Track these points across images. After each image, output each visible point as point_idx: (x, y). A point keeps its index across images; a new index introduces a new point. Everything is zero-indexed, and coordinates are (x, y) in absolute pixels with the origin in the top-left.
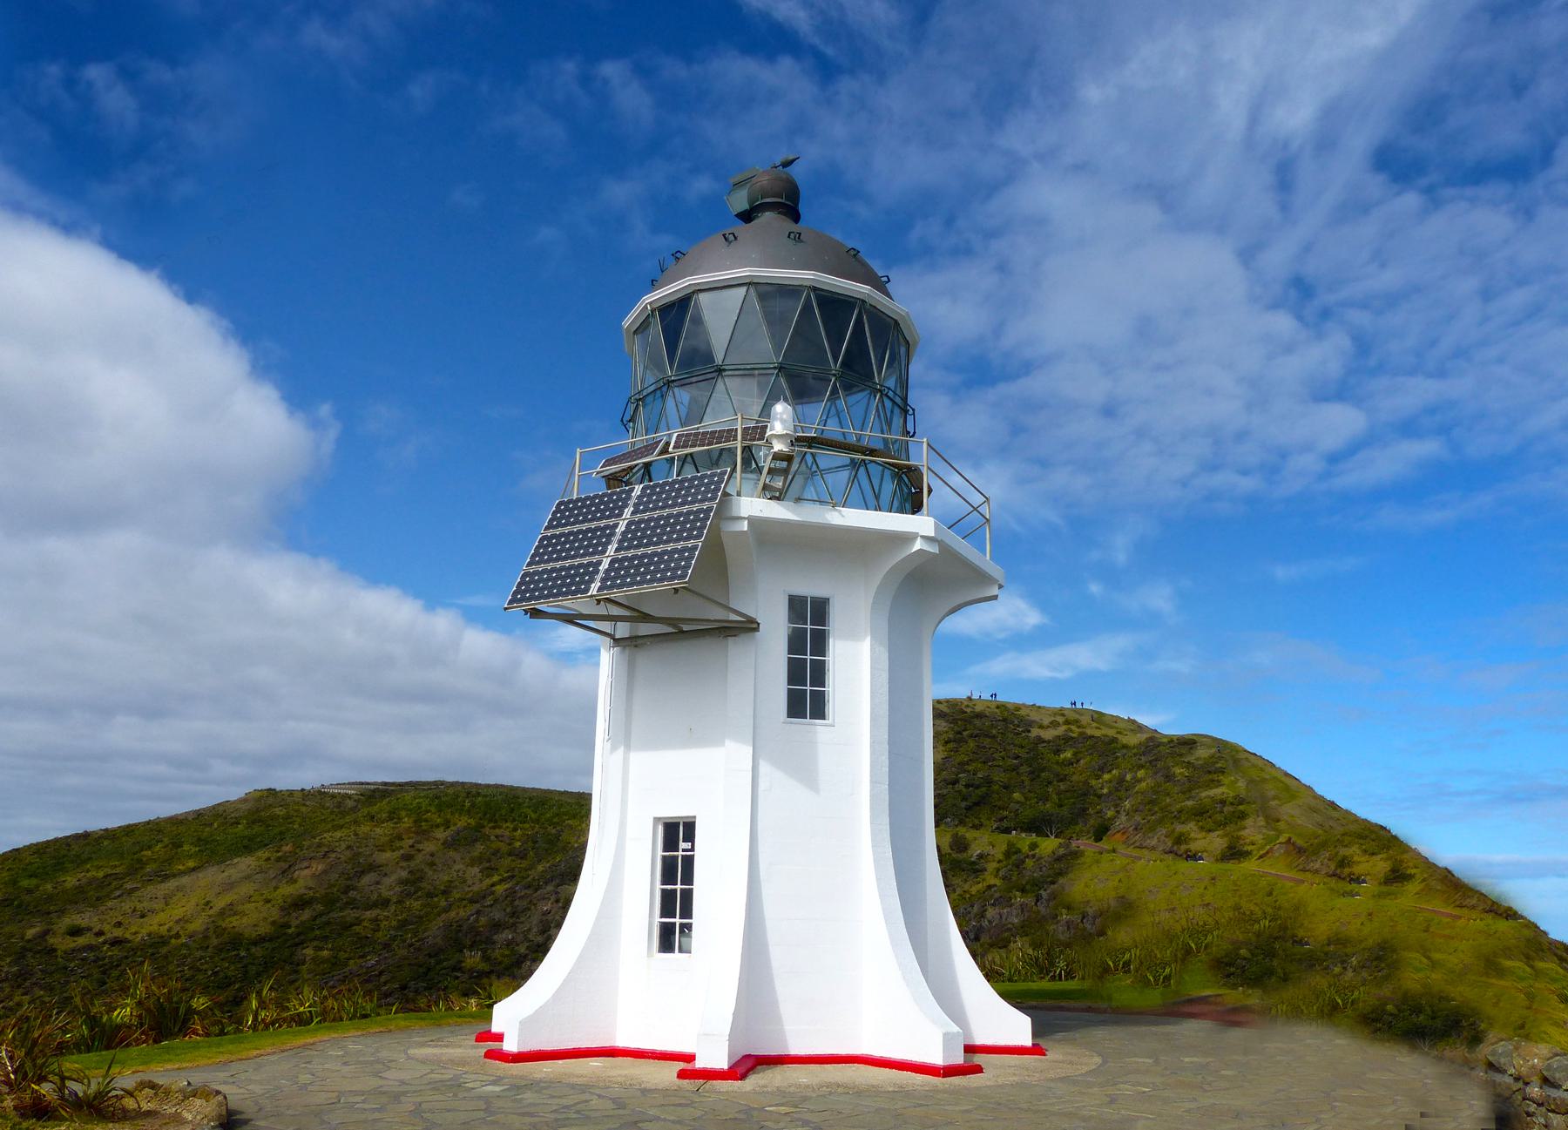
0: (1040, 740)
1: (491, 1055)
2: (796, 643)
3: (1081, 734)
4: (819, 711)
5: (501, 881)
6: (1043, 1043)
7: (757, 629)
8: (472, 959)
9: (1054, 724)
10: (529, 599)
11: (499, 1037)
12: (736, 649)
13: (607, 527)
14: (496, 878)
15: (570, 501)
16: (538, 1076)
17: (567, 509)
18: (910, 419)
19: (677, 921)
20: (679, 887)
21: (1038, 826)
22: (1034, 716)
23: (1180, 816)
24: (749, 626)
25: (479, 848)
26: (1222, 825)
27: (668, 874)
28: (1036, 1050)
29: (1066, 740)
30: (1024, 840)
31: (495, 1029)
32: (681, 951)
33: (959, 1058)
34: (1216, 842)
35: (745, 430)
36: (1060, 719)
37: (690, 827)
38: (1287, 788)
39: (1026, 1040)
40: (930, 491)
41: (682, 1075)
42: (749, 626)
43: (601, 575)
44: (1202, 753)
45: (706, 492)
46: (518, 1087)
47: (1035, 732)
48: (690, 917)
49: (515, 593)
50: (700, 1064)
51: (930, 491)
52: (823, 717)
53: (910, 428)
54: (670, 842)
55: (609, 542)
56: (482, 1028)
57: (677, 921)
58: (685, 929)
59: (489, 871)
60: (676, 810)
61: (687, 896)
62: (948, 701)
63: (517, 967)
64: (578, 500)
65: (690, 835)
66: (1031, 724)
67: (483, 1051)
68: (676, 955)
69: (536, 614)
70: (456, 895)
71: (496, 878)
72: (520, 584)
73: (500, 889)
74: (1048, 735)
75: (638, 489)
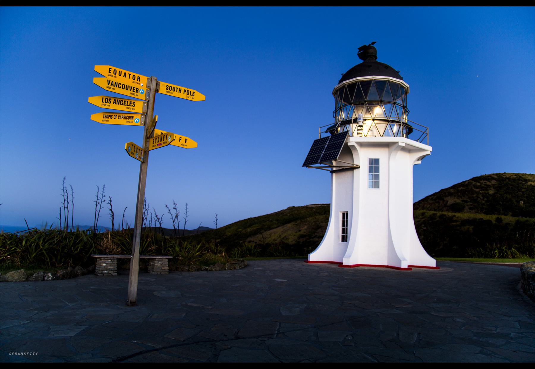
2: (371, 170)
24: (358, 167)
33: (407, 267)
37: (347, 214)
42: (358, 167)
47: (530, 183)
54: (343, 218)
65: (378, 164)
66: (529, 180)
69: (309, 167)
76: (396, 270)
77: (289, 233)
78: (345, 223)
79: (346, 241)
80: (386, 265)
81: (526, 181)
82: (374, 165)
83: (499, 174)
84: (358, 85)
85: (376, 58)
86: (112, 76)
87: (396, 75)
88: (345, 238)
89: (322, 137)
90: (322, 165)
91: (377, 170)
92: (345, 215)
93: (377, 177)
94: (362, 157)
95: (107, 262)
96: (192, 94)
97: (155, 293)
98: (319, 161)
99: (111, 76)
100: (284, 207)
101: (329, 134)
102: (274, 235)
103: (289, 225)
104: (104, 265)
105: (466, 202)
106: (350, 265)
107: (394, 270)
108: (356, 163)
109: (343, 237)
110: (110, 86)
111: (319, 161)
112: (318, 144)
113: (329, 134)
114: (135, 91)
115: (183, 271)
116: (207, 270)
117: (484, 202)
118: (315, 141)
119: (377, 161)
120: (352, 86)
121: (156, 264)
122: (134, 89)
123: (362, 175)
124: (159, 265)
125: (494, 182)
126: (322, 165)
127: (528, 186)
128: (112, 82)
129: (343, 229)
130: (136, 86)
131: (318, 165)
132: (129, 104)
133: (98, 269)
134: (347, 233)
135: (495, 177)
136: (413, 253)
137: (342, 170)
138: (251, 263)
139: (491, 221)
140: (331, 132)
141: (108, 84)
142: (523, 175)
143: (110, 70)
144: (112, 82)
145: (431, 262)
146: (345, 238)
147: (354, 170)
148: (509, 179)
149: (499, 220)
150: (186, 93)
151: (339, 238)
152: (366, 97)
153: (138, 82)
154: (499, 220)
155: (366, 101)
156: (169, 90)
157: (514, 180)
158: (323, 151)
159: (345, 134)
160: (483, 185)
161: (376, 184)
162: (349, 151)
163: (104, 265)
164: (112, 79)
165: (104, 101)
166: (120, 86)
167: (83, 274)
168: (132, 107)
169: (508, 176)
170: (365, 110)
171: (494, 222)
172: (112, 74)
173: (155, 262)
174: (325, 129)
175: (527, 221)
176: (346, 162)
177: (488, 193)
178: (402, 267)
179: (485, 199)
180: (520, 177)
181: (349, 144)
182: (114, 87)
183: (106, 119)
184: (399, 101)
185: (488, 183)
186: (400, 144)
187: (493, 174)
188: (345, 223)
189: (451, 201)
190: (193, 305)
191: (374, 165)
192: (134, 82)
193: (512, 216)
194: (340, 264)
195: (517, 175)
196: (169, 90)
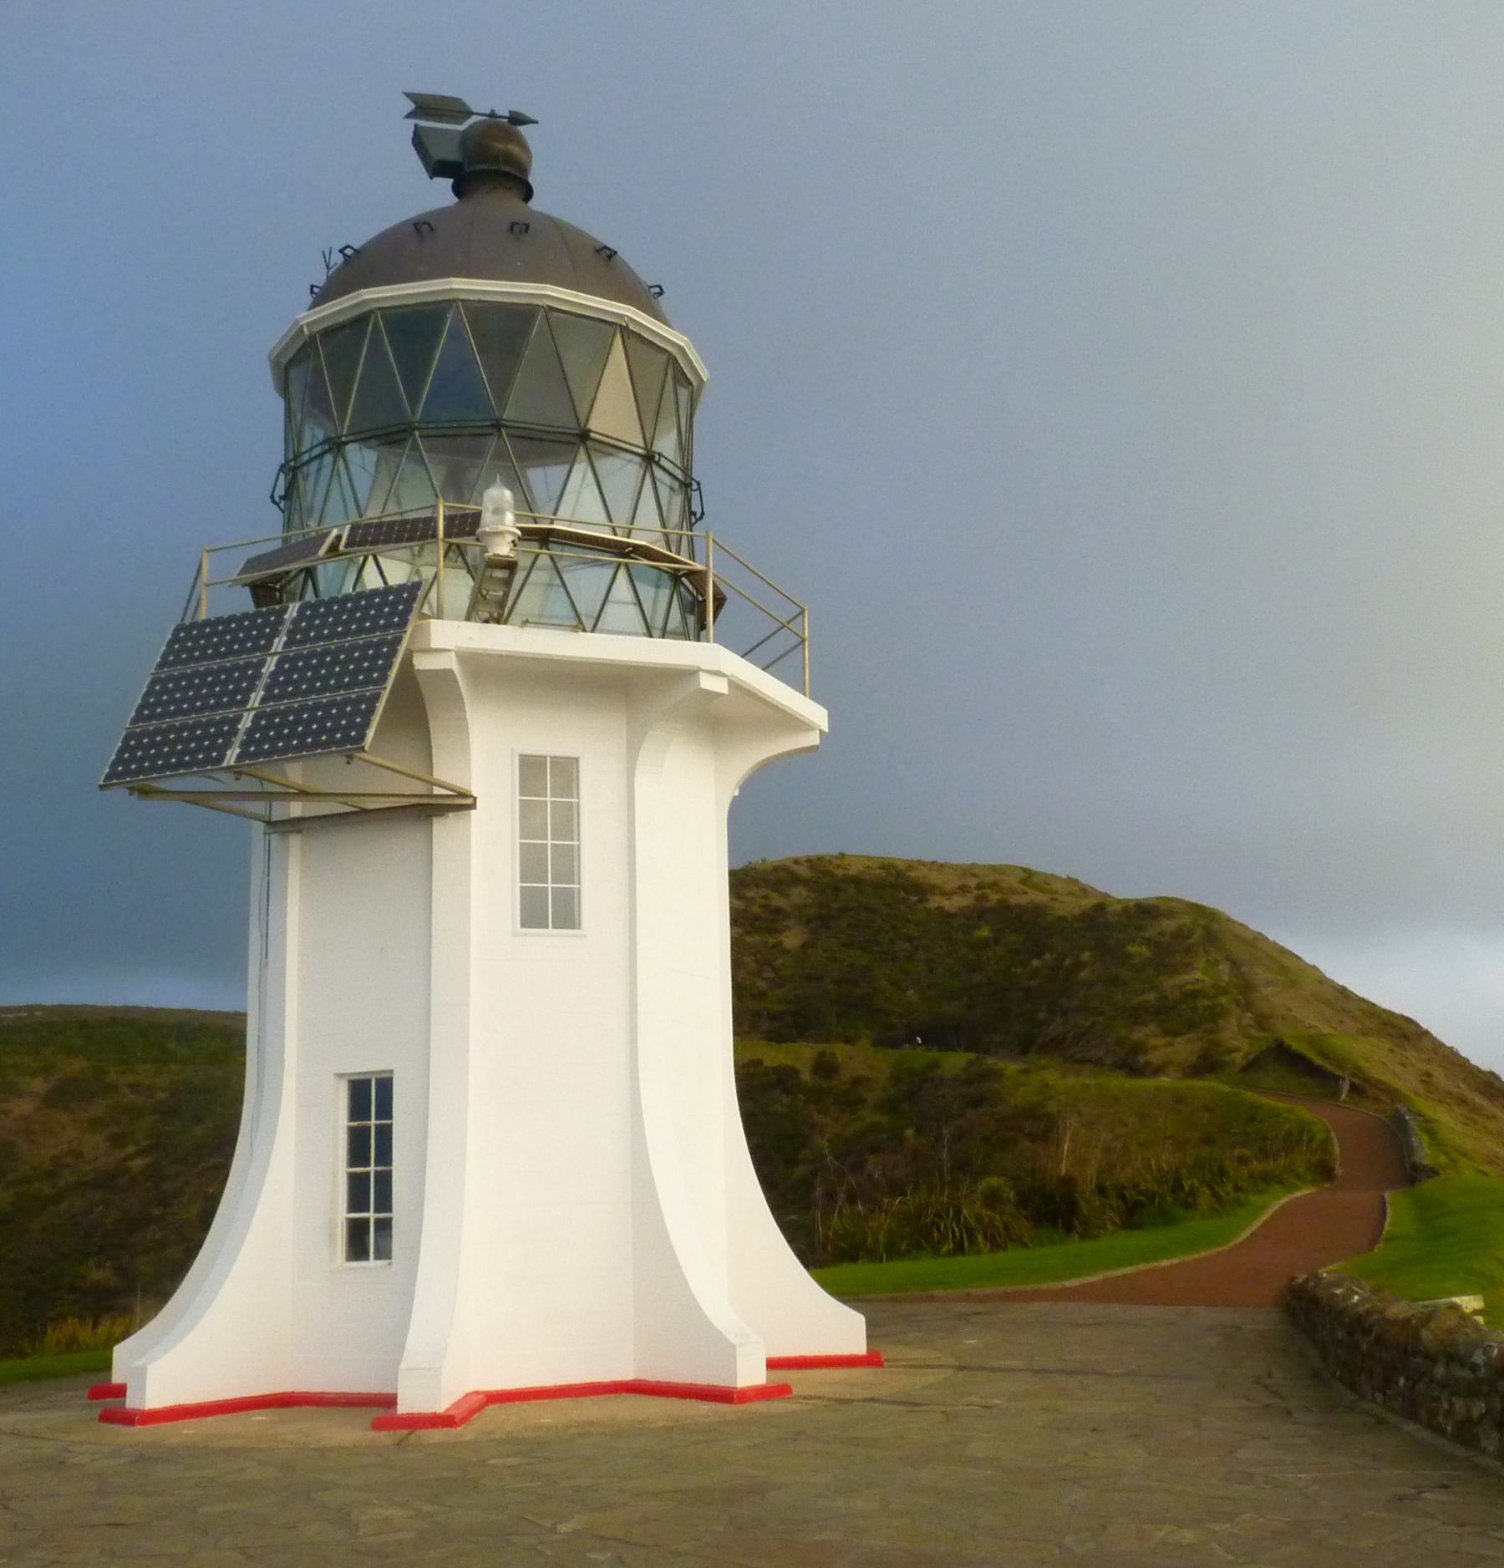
0: (945, 916)
1: (108, 1417)
3: (1000, 902)
4: (567, 915)
5: (139, 1153)
6: (887, 1352)
8: (99, 1274)
9: (963, 889)
10: (136, 773)
11: (121, 1391)
12: (443, 829)
13: (248, 666)
14: (131, 1149)
15: (193, 625)
16: (174, 1441)
17: (189, 637)
18: (695, 496)
19: (372, 1215)
20: (372, 1169)
21: (940, 1036)
22: (934, 878)
23: (1136, 1016)
24: (460, 803)
25: (99, 1107)
26: (1191, 1026)
27: (358, 1149)
28: (870, 1360)
29: (979, 914)
30: (918, 1056)
31: (117, 1378)
32: (378, 1257)
34: (1184, 1048)
35: (449, 520)
36: (973, 882)
37: (385, 1085)
38: (1284, 970)
39: (860, 1348)
40: (720, 601)
41: (378, 1425)
42: (460, 803)
43: (240, 737)
44: (1169, 925)
45: (392, 614)
46: (143, 1458)
47: (935, 902)
48: (389, 1209)
49: (115, 764)
50: (403, 1408)
51: (720, 601)
52: (567, 915)
53: (696, 507)
54: (358, 1108)
55: (252, 688)
56: (96, 1380)
57: (372, 1215)
58: (384, 1226)
59: (117, 1140)
60: (367, 1064)
61: (385, 1180)
62: (809, 861)
64: (207, 623)
65: (385, 1110)
66: (933, 889)
67: (97, 1412)
68: (372, 1262)
69: (145, 792)
70: (68, 1177)
71: (131, 1149)
72: (121, 752)
73: (138, 1164)
74: (954, 904)
75: (293, 610)
76: (705, 1407)
79: (384, 1253)
80: (627, 1374)
81: (922, 890)
83: (820, 858)
85: (528, 193)
87: (647, 298)
92: (370, 1099)
94: (484, 753)
108: (447, 772)
117: (761, 984)
119: (566, 770)
120: (416, 327)
123: (482, 854)
125: (799, 895)
127: (928, 911)
135: (804, 871)
136: (756, 1300)
137: (360, 817)
139: (794, 1072)
142: (911, 865)
145: (841, 1329)
148: (856, 881)
149: (825, 1068)
151: (332, 1238)
152: (502, 392)
154: (825, 1068)
155: (497, 425)
157: (878, 886)
160: (756, 909)
161: (549, 902)
169: (853, 871)
170: (438, 476)
171: (806, 1076)
175: (935, 1065)
176: (379, 771)
177: (777, 945)
179: (769, 974)
180: (899, 874)
181: (422, 663)
185: (777, 901)
187: (796, 862)
193: (877, 1043)
195: (887, 866)
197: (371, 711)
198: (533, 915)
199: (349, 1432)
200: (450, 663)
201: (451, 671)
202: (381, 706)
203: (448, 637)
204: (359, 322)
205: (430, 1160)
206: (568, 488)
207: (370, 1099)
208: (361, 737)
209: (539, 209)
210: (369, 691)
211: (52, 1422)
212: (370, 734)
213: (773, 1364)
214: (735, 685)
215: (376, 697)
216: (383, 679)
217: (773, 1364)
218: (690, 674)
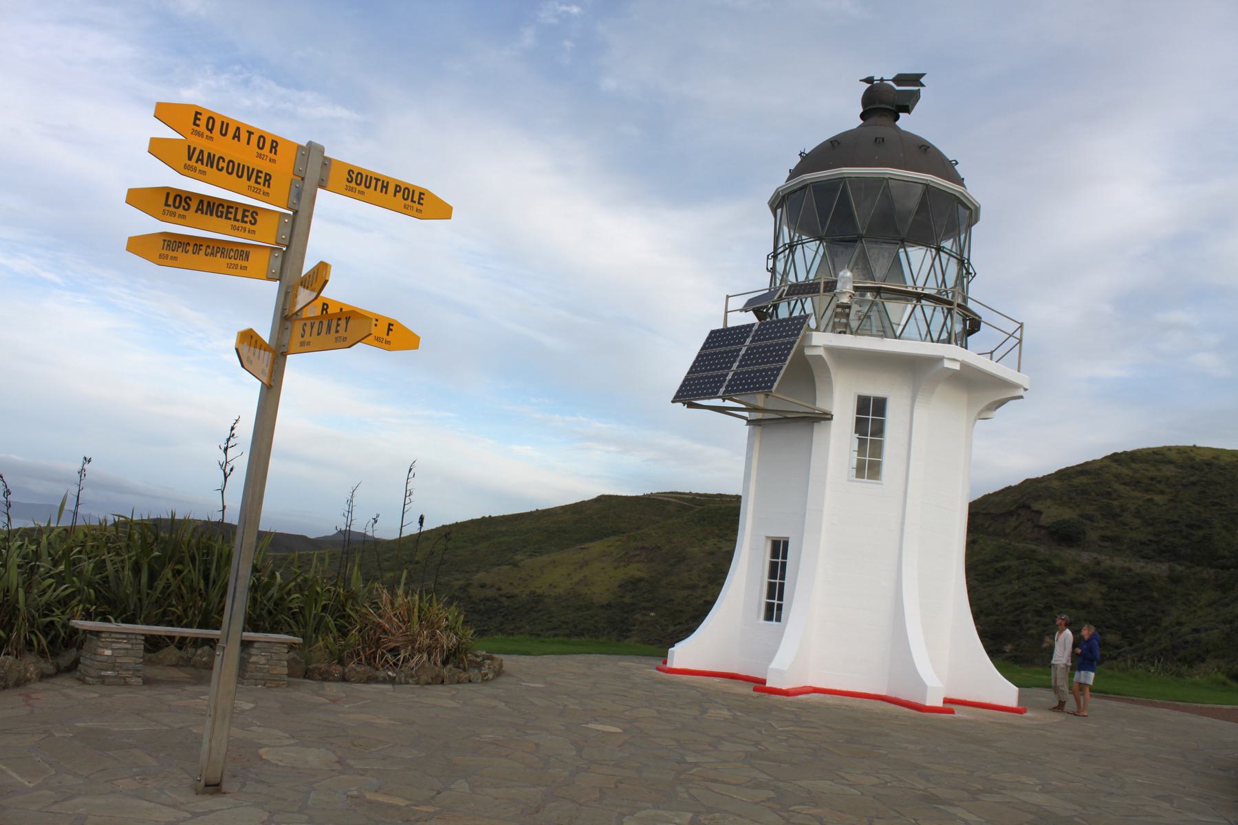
2: (860, 426)
7: (831, 419)
24: (826, 417)
33: (940, 704)
37: (786, 543)
42: (826, 417)
54: (775, 554)
57: (776, 602)
58: (780, 607)
60: (779, 534)
63: (689, 615)
68: (774, 623)
77: (599, 573)
78: (777, 570)
79: (779, 620)
82: (870, 415)
84: (844, 191)
86: (202, 135)
88: (773, 612)
89: (729, 325)
90: (728, 403)
91: (879, 430)
92: (779, 548)
93: (877, 449)
95: (114, 645)
96: (416, 199)
97: (262, 751)
98: (722, 390)
99: (201, 135)
100: (589, 491)
101: (750, 318)
102: (554, 575)
103: (596, 547)
104: (108, 652)
105: (1090, 518)
106: (784, 688)
107: (906, 710)
108: (821, 405)
109: (770, 607)
110: (193, 163)
111: (722, 390)
112: (720, 343)
113: (750, 318)
114: (261, 181)
115: (325, 679)
116: (392, 681)
118: (712, 332)
119: (880, 405)
121: (253, 659)
122: (258, 177)
123: (838, 440)
124: (263, 661)
126: (728, 403)
128: (202, 152)
129: (771, 587)
130: (264, 166)
131: (717, 402)
132: (239, 217)
133: (88, 662)
134: (781, 598)
135: (1173, 456)
136: (947, 658)
138: (509, 661)
140: (757, 312)
141: (190, 159)
143: (196, 119)
144: (202, 152)
145: (1004, 692)
146: (773, 612)
147: (816, 426)
150: (400, 195)
153: (272, 156)
156: (353, 184)
158: (735, 365)
159: (797, 324)
161: (869, 467)
162: (808, 374)
163: (108, 652)
164: (200, 143)
165: (170, 202)
166: (221, 164)
167: (43, 676)
168: (248, 226)
172: (203, 128)
173: (254, 651)
174: (742, 301)
178: (928, 704)
182: (203, 168)
183: (171, 254)
184: (947, 244)
186: (947, 364)
188: (777, 570)
189: (1052, 513)
190: (381, 798)
191: (870, 415)
192: (259, 156)
194: (759, 684)
196: (353, 184)
197: (778, 375)
198: (860, 470)
199: (747, 689)
200: (821, 352)
201: (820, 356)
202: (782, 372)
203: (821, 341)
204: (804, 188)
205: (799, 579)
206: (296, 232)
207: (779, 548)
208: (771, 386)
209: (903, 128)
210: (724, 372)
211: (640, 668)
212: (776, 384)
213: (946, 701)
214: (964, 365)
215: (781, 368)
216: (785, 360)
217: (946, 701)
218: (940, 359)
